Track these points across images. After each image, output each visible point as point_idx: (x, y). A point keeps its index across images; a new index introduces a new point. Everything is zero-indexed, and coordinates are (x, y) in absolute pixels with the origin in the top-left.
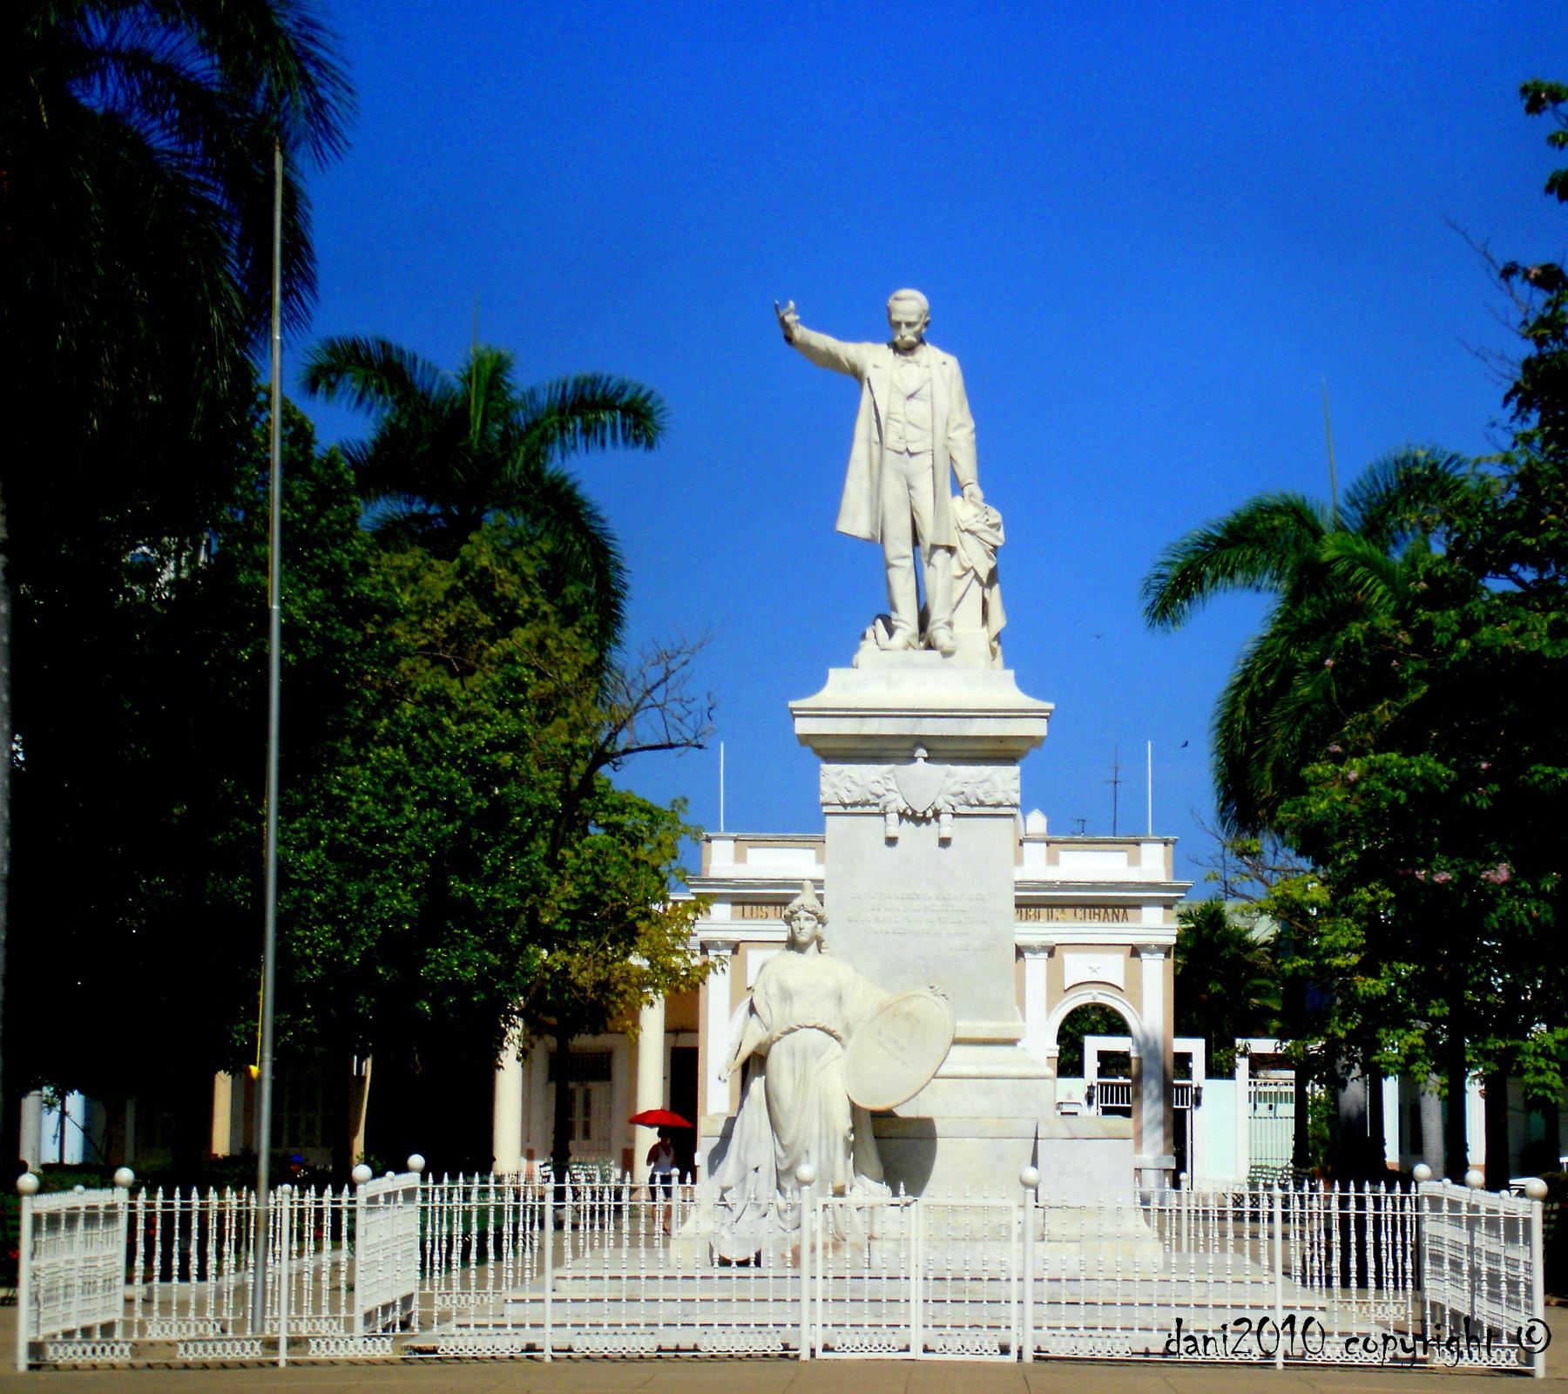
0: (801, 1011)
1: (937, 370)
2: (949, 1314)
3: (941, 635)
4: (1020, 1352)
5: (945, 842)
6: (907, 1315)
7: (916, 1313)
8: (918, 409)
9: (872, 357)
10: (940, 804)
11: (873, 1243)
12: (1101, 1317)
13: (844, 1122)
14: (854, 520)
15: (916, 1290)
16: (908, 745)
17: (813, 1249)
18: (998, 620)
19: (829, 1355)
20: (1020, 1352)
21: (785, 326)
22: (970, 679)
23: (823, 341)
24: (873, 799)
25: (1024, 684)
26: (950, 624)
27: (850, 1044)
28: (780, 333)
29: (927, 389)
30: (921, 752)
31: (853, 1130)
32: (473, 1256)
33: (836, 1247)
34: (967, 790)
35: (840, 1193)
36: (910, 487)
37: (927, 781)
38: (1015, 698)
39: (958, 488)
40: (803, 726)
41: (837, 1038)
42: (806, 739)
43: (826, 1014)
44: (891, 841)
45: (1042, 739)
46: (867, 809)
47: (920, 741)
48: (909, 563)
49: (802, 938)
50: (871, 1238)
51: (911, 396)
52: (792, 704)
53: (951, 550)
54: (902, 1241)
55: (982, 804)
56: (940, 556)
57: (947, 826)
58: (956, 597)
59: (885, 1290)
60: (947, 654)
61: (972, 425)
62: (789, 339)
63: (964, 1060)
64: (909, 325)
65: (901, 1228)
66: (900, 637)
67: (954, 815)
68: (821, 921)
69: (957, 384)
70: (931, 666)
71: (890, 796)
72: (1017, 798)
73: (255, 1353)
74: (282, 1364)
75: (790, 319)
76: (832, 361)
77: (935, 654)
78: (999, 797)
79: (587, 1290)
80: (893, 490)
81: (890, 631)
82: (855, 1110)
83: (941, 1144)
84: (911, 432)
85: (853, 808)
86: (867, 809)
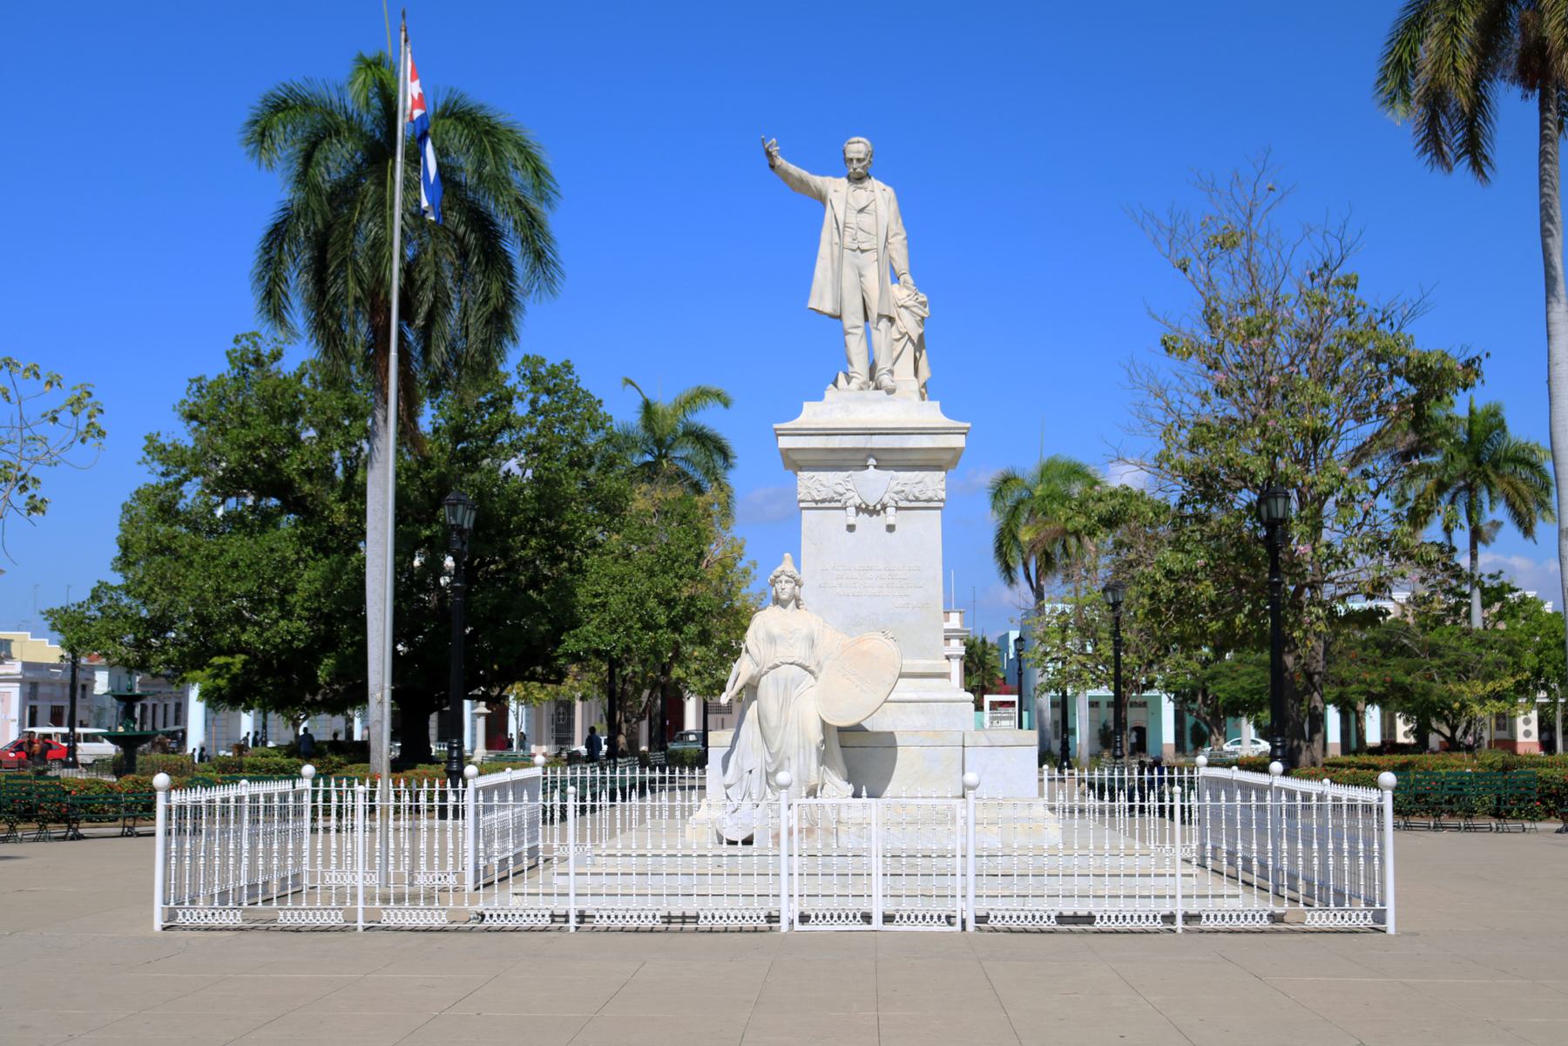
0: (782, 653)
1: (879, 194)
2: (903, 885)
3: (885, 380)
4: (963, 922)
5: (890, 528)
6: (870, 886)
7: (878, 885)
8: (865, 219)
9: (836, 189)
10: (885, 500)
11: (841, 828)
12: (1017, 886)
13: (816, 736)
14: (821, 299)
15: (876, 865)
16: (862, 456)
17: (790, 833)
18: (925, 373)
19: (806, 927)
20: (963, 922)
21: (769, 154)
22: (906, 409)
23: (793, 169)
24: (837, 497)
25: (946, 411)
26: (891, 372)
27: (821, 676)
28: (766, 161)
29: (871, 207)
30: (872, 461)
31: (824, 741)
32: (436, 861)
33: (810, 831)
34: (907, 489)
35: (812, 792)
36: (861, 276)
37: (874, 483)
38: (941, 420)
39: (896, 278)
40: (785, 442)
41: (811, 672)
42: (786, 452)
43: (799, 653)
44: (851, 528)
45: (962, 449)
46: (833, 505)
47: (871, 452)
48: (860, 331)
49: (784, 597)
50: (839, 822)
51: (861, 211)
52: (776, 426)
53: (891, 320)
54: (862, 826)
55: (917, 500)
56: (884, 324)
57: (891, 516)
58: (895, 354)
59: (851, 865)
60: (891, 391)
61: (904, 234)
62: (772, 167)
63: (907, 689)
64: (859, 160)
65: (869, 823)
66: (854, 384)
67: (898, 508)
68: (798, 583)
69: (894, 205)
70: (878, 401)
71: (849, 494)
72: (943, 495)
73: (336, 919)
74: (360, 929)
75: (774, 150)
76: (802, 185)
77: (882, 393)
78: (930, 494)
79: (619, 865)
80: (849, 277)
81: (849, 379)
82: (825, 726)
83: (901, 753)
84: (861, 236)
85: (821, 504)
86: (833, 505)
